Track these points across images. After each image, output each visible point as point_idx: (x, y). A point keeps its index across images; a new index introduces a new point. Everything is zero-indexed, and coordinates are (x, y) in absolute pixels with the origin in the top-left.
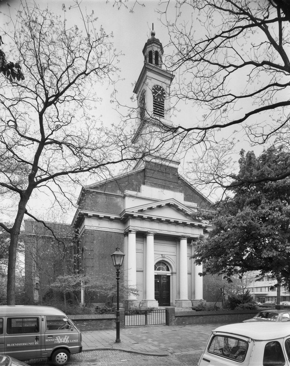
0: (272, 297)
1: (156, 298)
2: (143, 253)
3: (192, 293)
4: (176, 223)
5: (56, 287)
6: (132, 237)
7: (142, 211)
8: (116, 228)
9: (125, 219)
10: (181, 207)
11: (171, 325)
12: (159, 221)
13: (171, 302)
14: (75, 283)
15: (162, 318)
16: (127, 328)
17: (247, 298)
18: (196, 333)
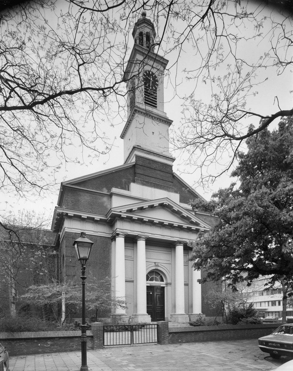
0: (272, 312)
1: (148, 312)
2: (131, 259)
3: (189, 306)
4: (171, 226)
5: (29, 299)
6: (120, 242)
7: (130, 211)
8: (101, 231)
9: (111, 221)
10: (176, 208)
11: (164, 344)
12: (151, 223)
13: (166, 316)
14: (50, 294)
15: (153, 335)
16: (107, 348)
17: (250, 312)
18: (196, 354)
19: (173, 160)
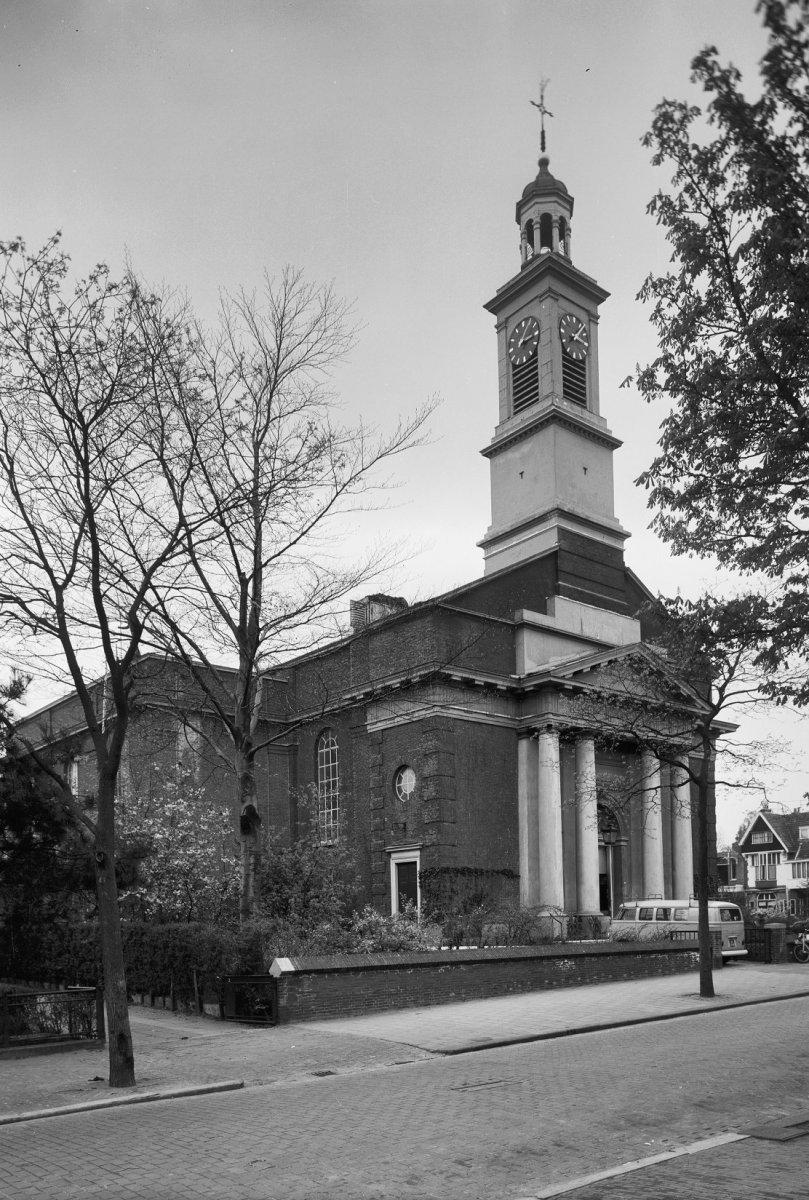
9: (522, 696)
19: (622, 536)
